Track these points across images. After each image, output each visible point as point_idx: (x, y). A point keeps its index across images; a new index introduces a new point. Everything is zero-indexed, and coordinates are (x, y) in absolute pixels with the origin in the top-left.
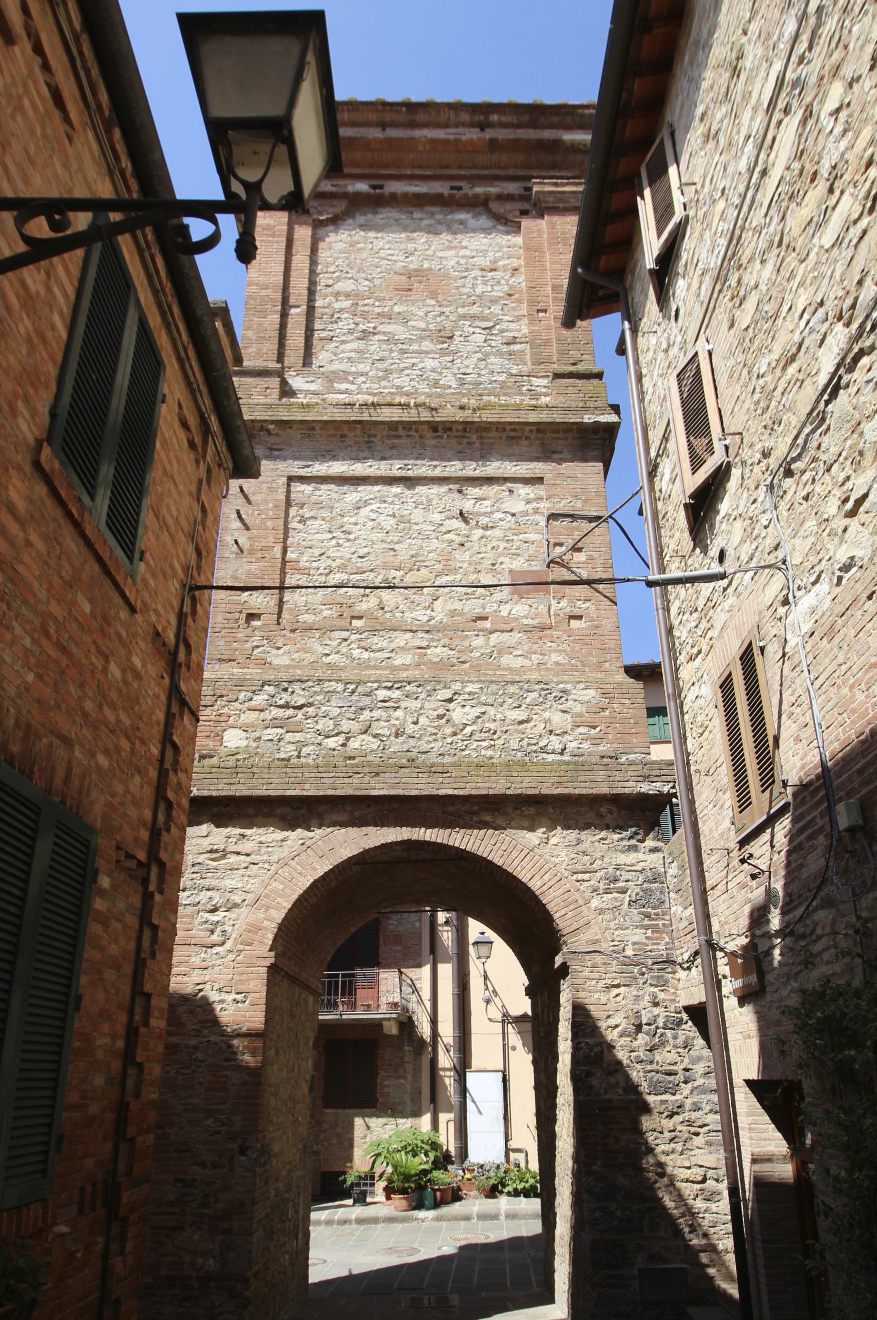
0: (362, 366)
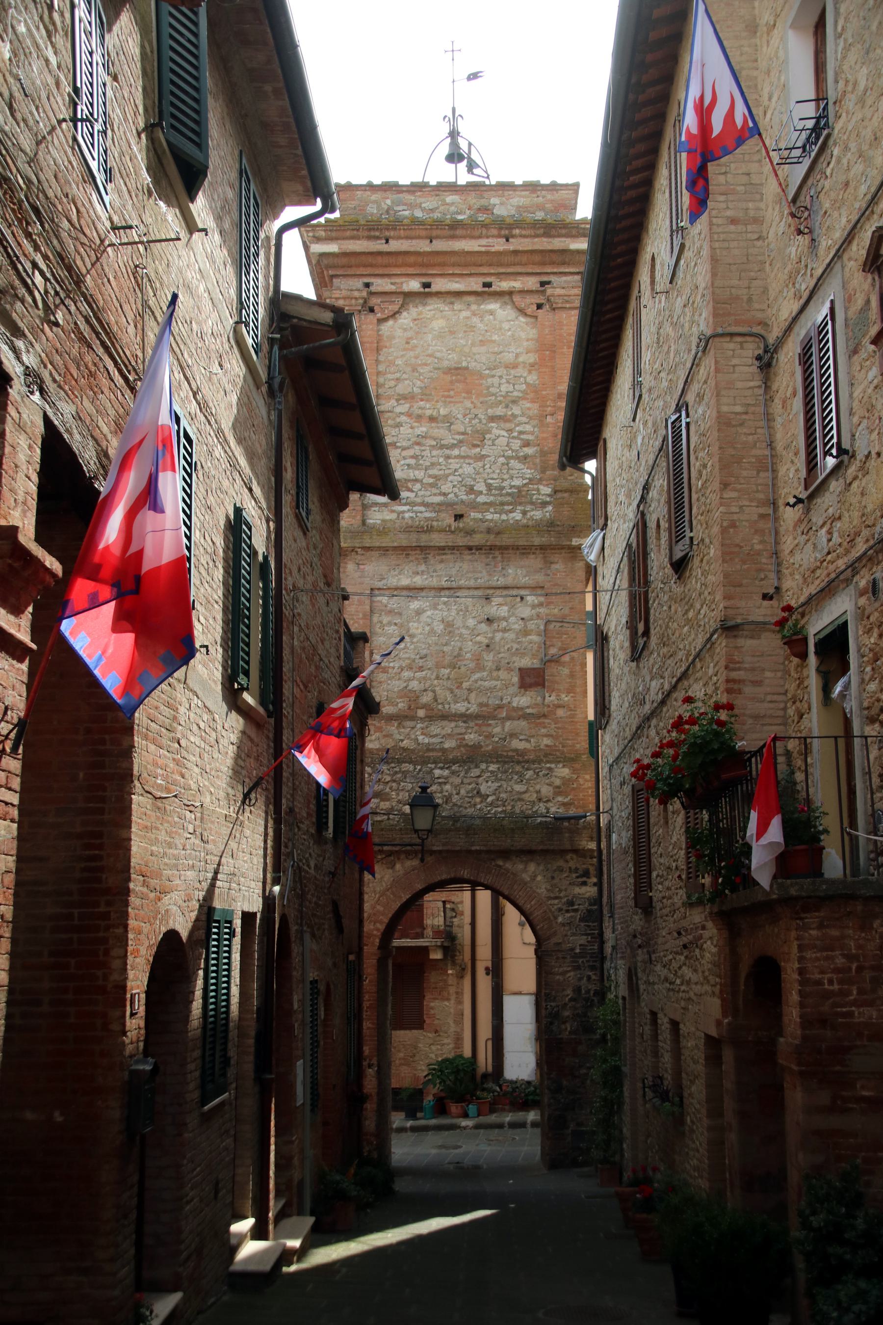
0: (417, 472)
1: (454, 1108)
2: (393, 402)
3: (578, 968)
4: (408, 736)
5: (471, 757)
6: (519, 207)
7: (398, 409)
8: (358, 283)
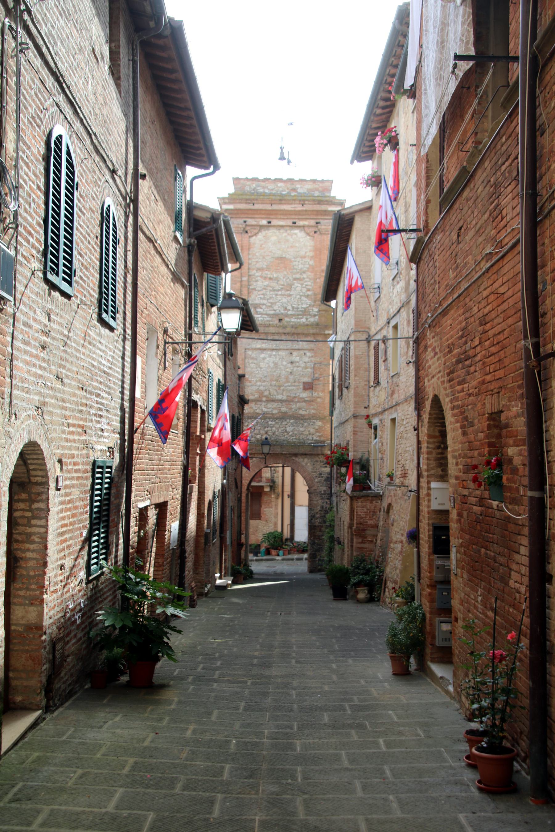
1: (273, 552)
2: (255, 271)
3: (323, 499)
5: (283, 417)
7: (257, 274)
8: (241, 221)
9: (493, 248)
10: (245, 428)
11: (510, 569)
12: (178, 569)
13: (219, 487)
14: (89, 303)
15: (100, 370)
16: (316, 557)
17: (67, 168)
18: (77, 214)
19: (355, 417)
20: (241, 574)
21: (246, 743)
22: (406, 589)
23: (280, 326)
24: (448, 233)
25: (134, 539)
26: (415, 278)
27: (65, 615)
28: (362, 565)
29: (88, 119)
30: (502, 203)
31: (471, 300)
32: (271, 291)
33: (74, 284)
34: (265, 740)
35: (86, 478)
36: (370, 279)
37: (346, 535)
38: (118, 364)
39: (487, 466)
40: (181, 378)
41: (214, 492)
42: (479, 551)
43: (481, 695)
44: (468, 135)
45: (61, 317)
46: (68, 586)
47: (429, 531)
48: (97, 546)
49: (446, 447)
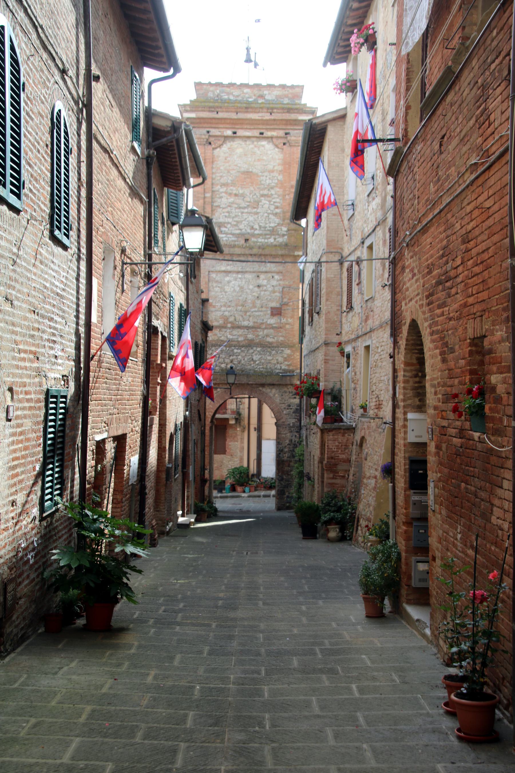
1: (239, 489)
2: (219, 187)
3: (291, 432)
4: (223, 335)
5: (250, 345)
6: (276, 96)
7: (221, 190)
8: (204, 131)
9: (478, 158)
10: (208, 356)
11: (492, 505)
12: (137, 505)
13: (181, 419)
14: (40, 219)
15: (53, 291)
16: (284, 494)
17: (12, 65)
18: (25, 118)
19: (326, 344)
20: (205, 511)
21: (210, 689)
22: (380, 527)
23: (246, 247)
24: (429, 143)
25: (90, 473)
26: (392, 193)
27: (17, 555)
28: (333, 502)
29: (32, 8)
30: (490, 108)
31: (453, 216)
32: (236, 208)
33: (23, 197)
34: (231, 686)
35: (39, 408)
36: (343, 195)
37: (316, 470)
38: (72, 286)
39: (468, 395)
40: (141, 302)
41: (176, 425)
42: (459, 486)
43: (460, 638)
44: (455, 30)
45: (10, 233)
46: (20, 524)
47: (405, 465)
48: (51, 481)
49: (424, 376)
